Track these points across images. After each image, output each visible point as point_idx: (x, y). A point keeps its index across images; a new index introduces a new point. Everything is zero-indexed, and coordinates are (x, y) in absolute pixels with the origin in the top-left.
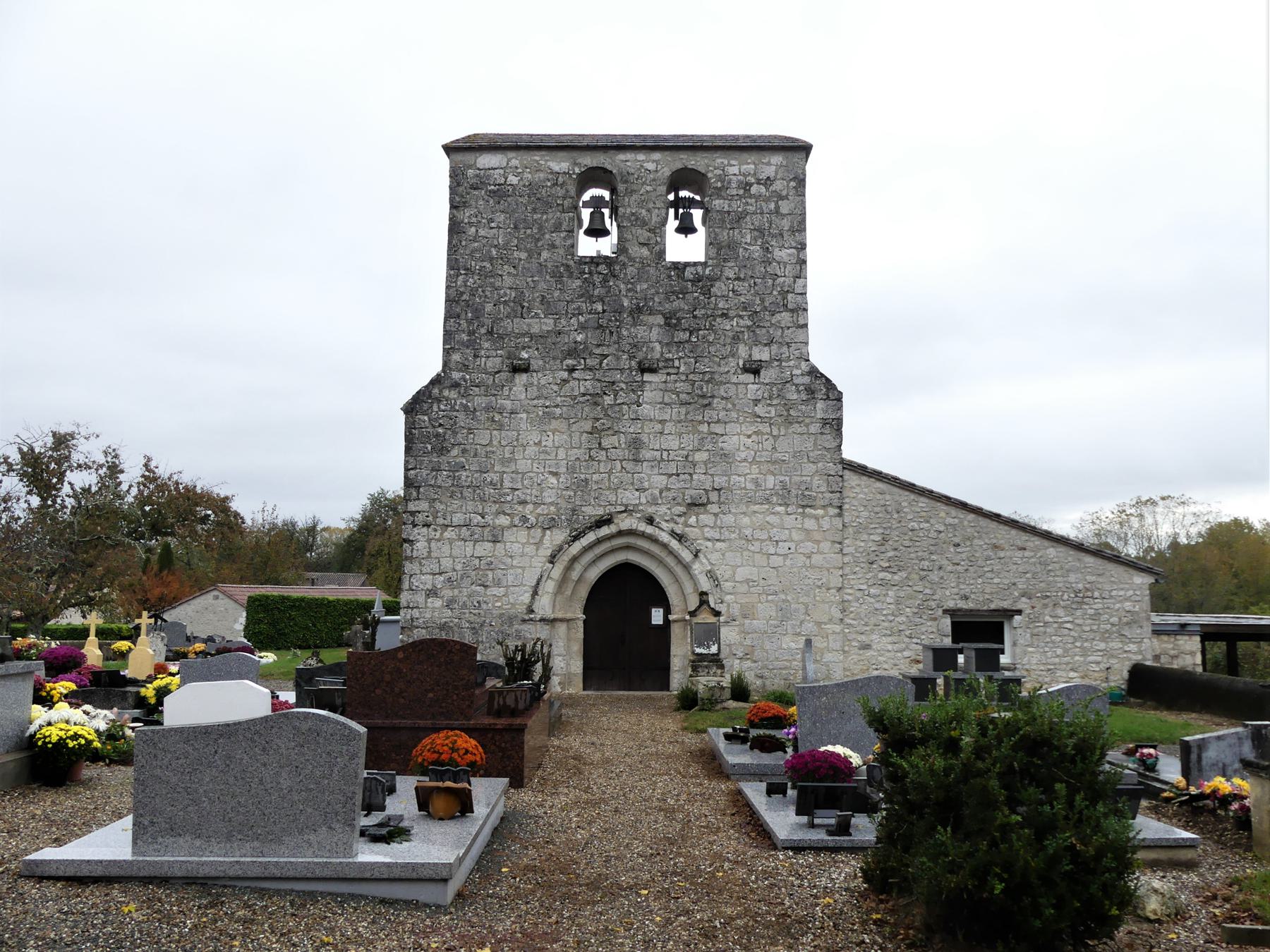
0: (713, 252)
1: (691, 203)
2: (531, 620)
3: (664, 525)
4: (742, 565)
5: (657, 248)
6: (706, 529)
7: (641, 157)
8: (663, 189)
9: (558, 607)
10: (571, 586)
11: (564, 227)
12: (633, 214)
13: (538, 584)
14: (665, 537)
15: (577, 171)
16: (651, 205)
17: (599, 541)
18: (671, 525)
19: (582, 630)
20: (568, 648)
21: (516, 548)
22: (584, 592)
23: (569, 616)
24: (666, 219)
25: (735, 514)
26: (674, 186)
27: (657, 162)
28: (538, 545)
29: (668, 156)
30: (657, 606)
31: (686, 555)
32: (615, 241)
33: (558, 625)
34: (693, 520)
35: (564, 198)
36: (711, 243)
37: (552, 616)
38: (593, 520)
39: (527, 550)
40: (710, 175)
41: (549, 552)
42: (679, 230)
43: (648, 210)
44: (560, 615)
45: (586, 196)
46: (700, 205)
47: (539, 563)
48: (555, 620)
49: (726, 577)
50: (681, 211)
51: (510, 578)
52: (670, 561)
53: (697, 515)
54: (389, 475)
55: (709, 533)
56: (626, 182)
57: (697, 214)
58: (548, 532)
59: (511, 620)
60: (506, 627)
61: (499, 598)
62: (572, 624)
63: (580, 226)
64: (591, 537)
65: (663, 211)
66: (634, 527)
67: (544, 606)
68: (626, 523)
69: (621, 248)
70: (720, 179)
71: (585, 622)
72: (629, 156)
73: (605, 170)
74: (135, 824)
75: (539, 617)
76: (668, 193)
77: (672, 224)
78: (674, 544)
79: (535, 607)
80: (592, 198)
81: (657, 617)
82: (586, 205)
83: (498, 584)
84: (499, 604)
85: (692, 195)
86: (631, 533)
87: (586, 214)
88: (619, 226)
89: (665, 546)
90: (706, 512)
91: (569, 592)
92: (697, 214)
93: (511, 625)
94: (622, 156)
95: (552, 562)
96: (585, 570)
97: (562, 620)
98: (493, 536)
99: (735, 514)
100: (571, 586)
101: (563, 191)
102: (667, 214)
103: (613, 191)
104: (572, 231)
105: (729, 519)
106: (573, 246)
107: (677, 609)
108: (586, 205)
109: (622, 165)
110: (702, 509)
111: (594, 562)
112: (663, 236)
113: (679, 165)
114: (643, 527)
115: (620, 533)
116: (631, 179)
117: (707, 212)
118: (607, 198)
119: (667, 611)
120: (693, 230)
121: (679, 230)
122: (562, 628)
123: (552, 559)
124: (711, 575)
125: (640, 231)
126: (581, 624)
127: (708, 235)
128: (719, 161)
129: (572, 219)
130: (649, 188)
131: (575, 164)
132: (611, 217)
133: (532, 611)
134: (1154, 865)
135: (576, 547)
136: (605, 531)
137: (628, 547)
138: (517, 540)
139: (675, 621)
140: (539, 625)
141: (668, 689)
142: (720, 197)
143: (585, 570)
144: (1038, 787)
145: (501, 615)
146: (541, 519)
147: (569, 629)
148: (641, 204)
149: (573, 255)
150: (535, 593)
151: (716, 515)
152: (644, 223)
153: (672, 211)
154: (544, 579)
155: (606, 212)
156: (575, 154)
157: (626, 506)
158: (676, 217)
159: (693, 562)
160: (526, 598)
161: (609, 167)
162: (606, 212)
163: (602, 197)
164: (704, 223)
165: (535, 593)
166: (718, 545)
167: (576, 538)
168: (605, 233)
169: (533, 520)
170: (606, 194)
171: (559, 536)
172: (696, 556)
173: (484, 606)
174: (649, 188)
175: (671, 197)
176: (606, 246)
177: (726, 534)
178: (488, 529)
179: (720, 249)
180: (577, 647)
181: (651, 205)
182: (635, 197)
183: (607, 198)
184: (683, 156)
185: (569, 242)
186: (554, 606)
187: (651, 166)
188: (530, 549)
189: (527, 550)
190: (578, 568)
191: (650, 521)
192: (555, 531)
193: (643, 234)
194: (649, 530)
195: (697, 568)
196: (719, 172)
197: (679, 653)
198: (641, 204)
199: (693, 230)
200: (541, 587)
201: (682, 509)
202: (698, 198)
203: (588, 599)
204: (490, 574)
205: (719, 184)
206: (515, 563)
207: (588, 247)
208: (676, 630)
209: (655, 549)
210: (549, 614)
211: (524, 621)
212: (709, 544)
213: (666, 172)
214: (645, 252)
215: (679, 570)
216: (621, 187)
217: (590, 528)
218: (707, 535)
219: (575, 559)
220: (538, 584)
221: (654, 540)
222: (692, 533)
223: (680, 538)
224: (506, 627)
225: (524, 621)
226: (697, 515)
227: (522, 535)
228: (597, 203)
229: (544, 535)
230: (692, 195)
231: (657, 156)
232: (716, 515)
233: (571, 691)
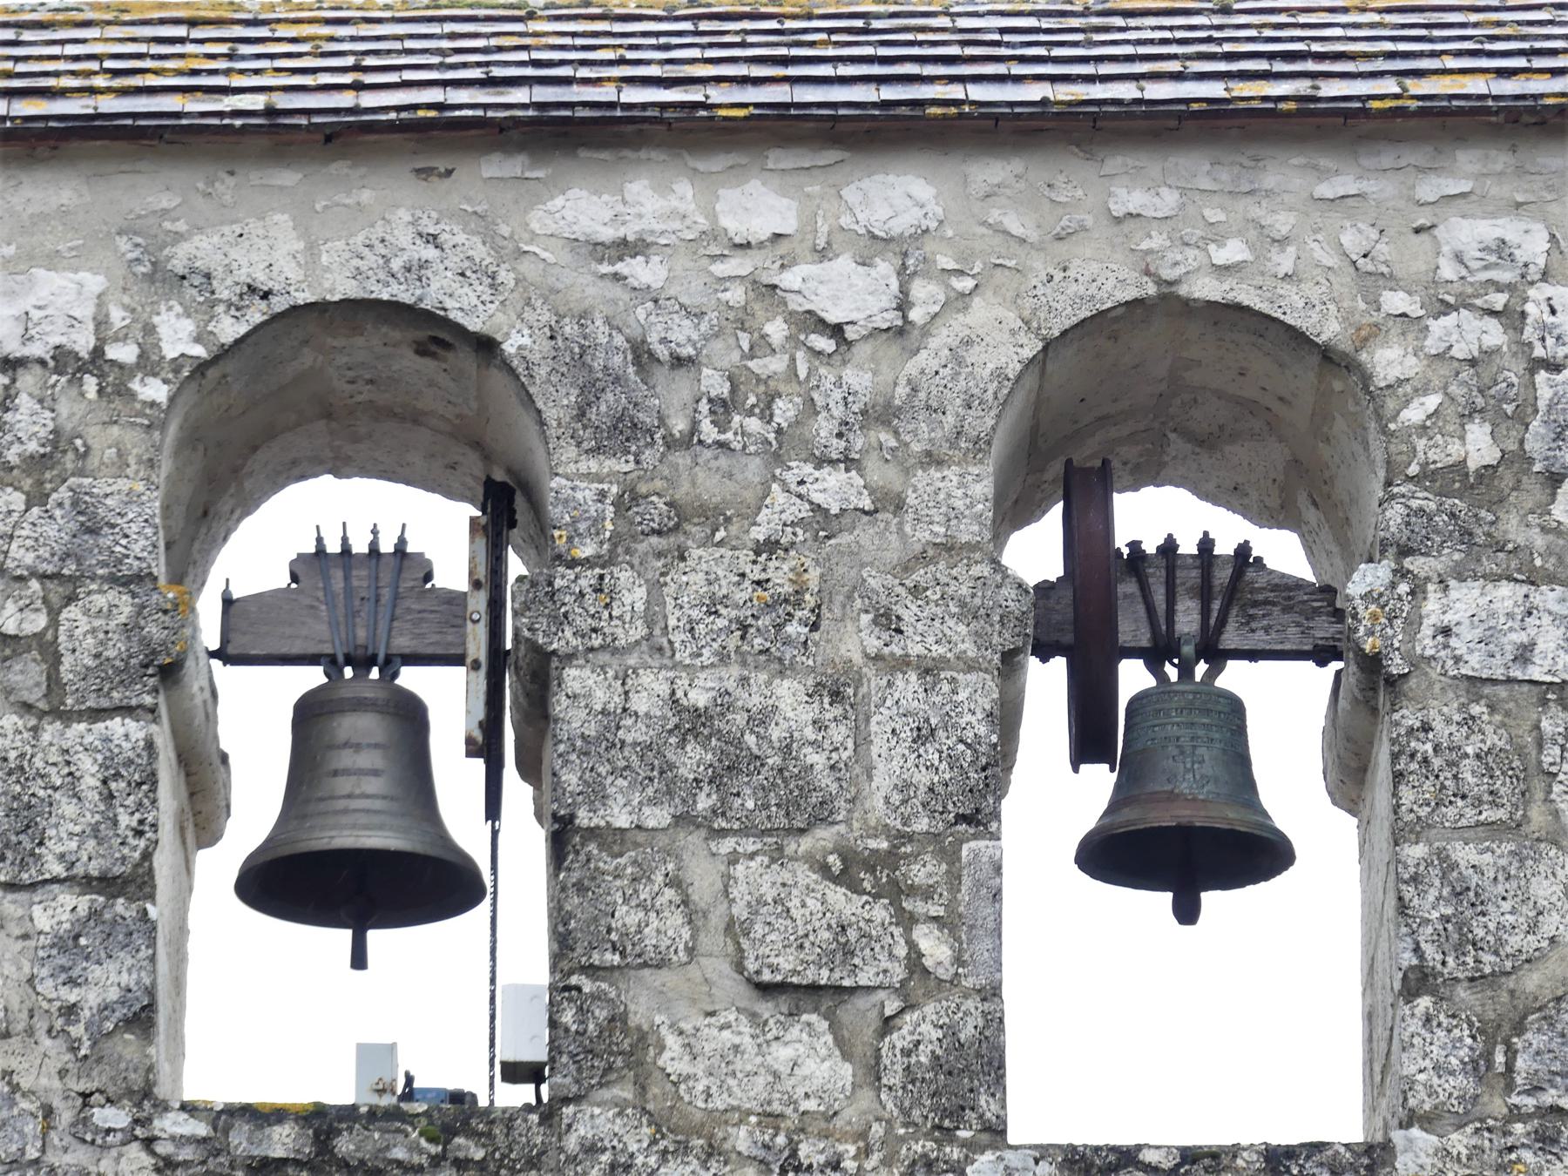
0: (1437, 1055)
1: (1229, 609)
5: (923, 1028)
7: (758, 203)
8: (971, 488)
11: (66, 837)
12: (693, 723)
15: (178, 337)
16: (855, 640)
24: (997, 762)
26: (1066, 446)
27: (903, 251)
29: (998, 196)
32: (529, 960)
35: (63, 585)
36: (1422, 970)
40: (1389, 361)
42: (1112, 855)
43: (833, 689)
45: (259, 552)
46: (1311, 623)
50: (1133, 678)
54: (914, 937)
56: (624, 432)
57: (1284, 708)
63: (204, 816)
65: (974, 695)
69: (590, 1040)
70: (1487, 392)
72: (649, 199)
73: (435, 334)
74: (1299, 584)
76: (1014, 510)
77: (1056, 797)
80: (315, 565)
82: (252, 636)
85: (1230, 530)
87: (255, 715)
88: (563, 837)
92: (1284, 708)
94: (584, 203)
101: (56, 529)
102: (1007, 717)
103: (505, 507)
104: (133, 883)
106: (141, 1017)
108: (252, 636)
109: (585, 285)
112: (975, 918)
113: (1105, 279)
116: (674, 399)
117: (1371, 687)
118: (453, 569)
120: (1257, 854)
121: (1112, 855)
125: (755, 877)
127: (1393, 901)
128: (1468, 233)
129: (130, 776)
130: (833, 488)
131: (164, 279)
132: (485, 746)
142: (1483, 555)
144: (1460, 1127)
148: (770, 627)
149: (144, 1096)
152: (799, 806)
153: (1047, 685)
155: (446, 696)
156: (155, 192)
158: (1090, 742)
161: (468, 307)
162: (446, 696)
163: (405, 564)
164: (1348, 775)
168: (433, 884)
170: (439, 530)
174: (833, 488)
175: (1037, 552)
176: (439, 1007)
179: (1499, 1032)
181: (855, 640)
182: (708, 567)
183: (453, 569)
184: (1142, 189)
185: (107, 982)
187: (851, 292)
193: (795, 905)
196: (1472, 333)
198: (770, 627)
199: (1257, 854)
202: (1283, 553)
205: (1479, 446)
207: (274, 1016)
213: (995, 341)
214: (809, 1061)
216: (576, 483)
228: (355, 619)
230: (1230, 530)
231: (898, 194)
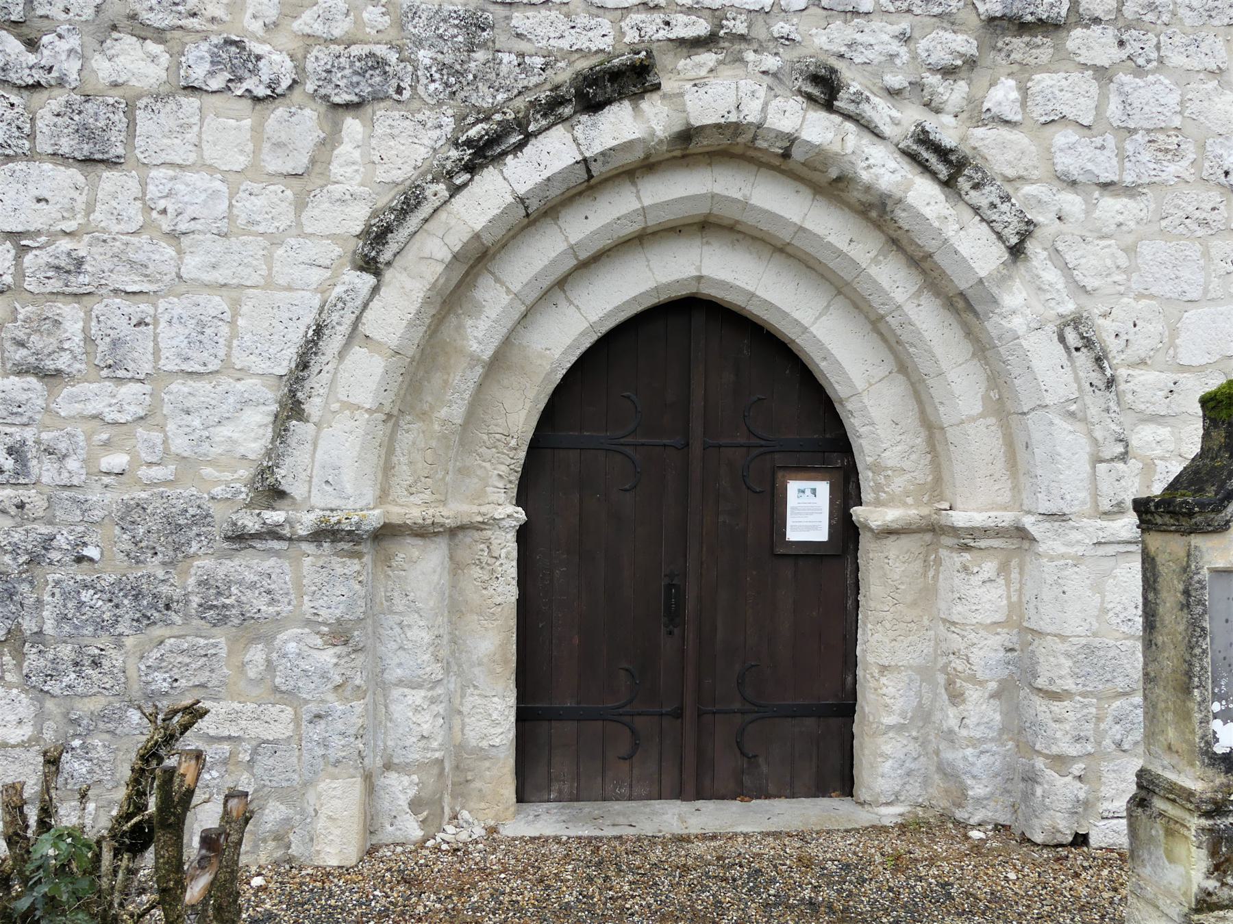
2: (273, 533)
3: (881, 111)
4: (1206, 299)
6: (1063, 137)
9: (404, 475)
10: (460, 383)
13: (304, 365)
14: (882, 168)
17: (590, 180)
18: (910, 116)
19: (510, 569)
20: (452, 652)
21: (196, 195)
22: (519, 413)
23: (454, 510)
25: (1184, 77)
28: (306, 179)
30: (806, 470)
31: (975, 250)
33: (408, 551)
34: (1003, 95)
37: (375, 518)
38: (563, 74)
39: (247, 206)
41: (356, 218)
44: (410, 509)
47: (308, 263)
48: (386, 534)
49: (1142, 345)
51: (172, 338)
52: (891, 280)
53: (1022, 73)
55: (1075, 153)
58: (352, 125)
59: (178, 532)
60: (154, 566)
61: (118, 431)
62: (471, 545)
64: (553, 153)
66: (751, 113)
67: (336, 470)
68: (709, 94)
71: (523, 535)
75: (307, 521)
78: (923, 196)
79: (284, 476)
81: (807, 512)
83: (114, 369)
84: (117, 460)
86: (730, 145)
89: (877, 212)
90: (1063, 58)
91: (455, 411)
93: (178, 557)
95: (369, 265)
96: (526, 317)
97: (423, 532)
98: (85, 133)
99: (1184, 77)
100: (460, 383)
105: (1154, 96)
107: (898, 484)
110: (1044, 49)
111: (561, 285)
114: (791, 117)
115: (690, 147)
119: (847, 492)
122: (424, 566)
123: (373, 252)
124: (1079, 336)
126: (507, 546)
133: (277, 494)
134: (1189, 795)
135: (490, 196)
136: (620, 126)
137: (708, 225)
138: (203, 155)
139: (889, 532)
140: (311, 558)
141: (838, 776)
143: (526, 317)
145: (129, 514)
146: (318, 60)
147: (456, 567)
150: (292, 408)
151: (1102, 74)
154: (332, 344)
157: (717, 15)
159: (1003, 279)
160: (250, 433)
165: (292, 408)
166: (1110, 206)
167: (483, 153)
169: (276, 63)
171: (403, 143)
172: (1017, 251)
173: (45, 471)
177: (1141, 167)
178: (56, 101)
180: (493, 639)
186: (388, 469)
188: (268, 204)
189: (247, 206)
190: (494, 303)
191: (824, 88)
192: (386, 117)
194: (817, 129)
195: (1023, 308)
197: (905, 657)
200: (317, 381)
201: (963, 43)
203: (537, 446)
204: (72, 317)
206: (192, 265)
208: (884, 574)
209: (827, 226)
210: (359, 504)
211: (240, 538)
212: (1071, 202)
215: (926, 320)
217: (552, 108)
218: (1067, 163)
219: (478, 259)
220: (304, 365)
221: (829, 182)
222: (998, 149)
223: (948, 165)
224: (154, 566)
225: (240, 538)
226: (1022, 73)
227: (227, 132)
229: (330, 142)
232: (1102, 74)
233: (468, 828)
